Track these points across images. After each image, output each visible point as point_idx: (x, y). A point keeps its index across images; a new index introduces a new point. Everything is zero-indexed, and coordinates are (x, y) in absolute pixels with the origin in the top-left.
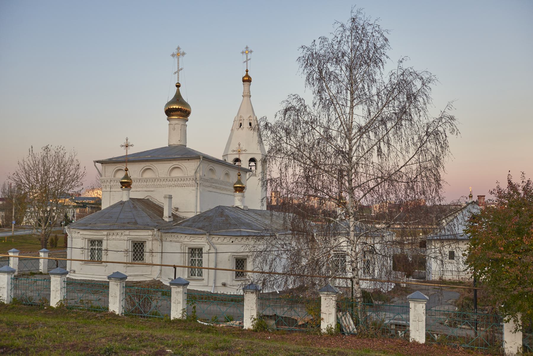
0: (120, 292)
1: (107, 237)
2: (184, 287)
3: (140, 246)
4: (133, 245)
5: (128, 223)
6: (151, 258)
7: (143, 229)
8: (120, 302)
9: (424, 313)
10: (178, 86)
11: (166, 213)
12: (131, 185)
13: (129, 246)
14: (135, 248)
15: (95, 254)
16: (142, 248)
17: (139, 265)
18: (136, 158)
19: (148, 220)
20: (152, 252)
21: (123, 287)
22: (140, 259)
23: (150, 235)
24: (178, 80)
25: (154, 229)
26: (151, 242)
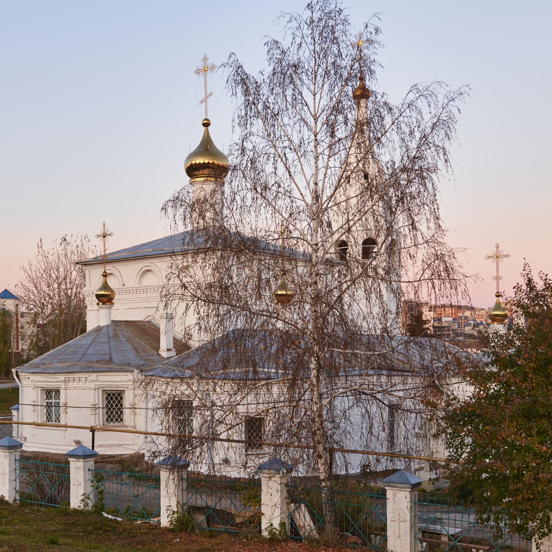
0: (10, 467)
1: (65, 384)
2: (86, 460)
3: (116, 398)
4: (105, 396)
5: (98, 361)
6: (132, 417)
7: (117, 371)
8: (10, 482)
9: (407, 508)
10: (206, 125)
11: (165, 343)
12: (112, 299)
13: (99, 399)
14: (109, 402)
15: (51, 411)
16: (119, 402)
17: (48, 428)
18: (132, 254)
19: (131, 356)
20: (133, 408)
21: (16, 460)
22: (117, 420)
23: (130, 381)
24: (206, 114)
25: (133, 371)
26: (132, 391)
